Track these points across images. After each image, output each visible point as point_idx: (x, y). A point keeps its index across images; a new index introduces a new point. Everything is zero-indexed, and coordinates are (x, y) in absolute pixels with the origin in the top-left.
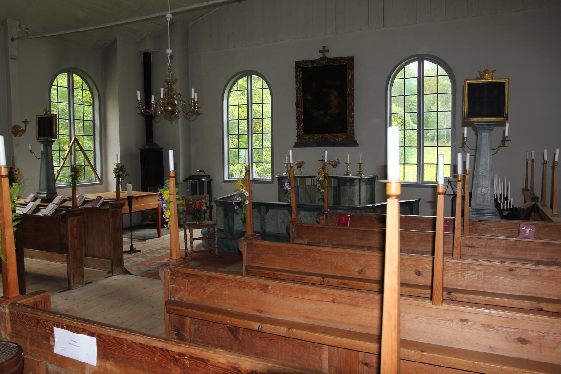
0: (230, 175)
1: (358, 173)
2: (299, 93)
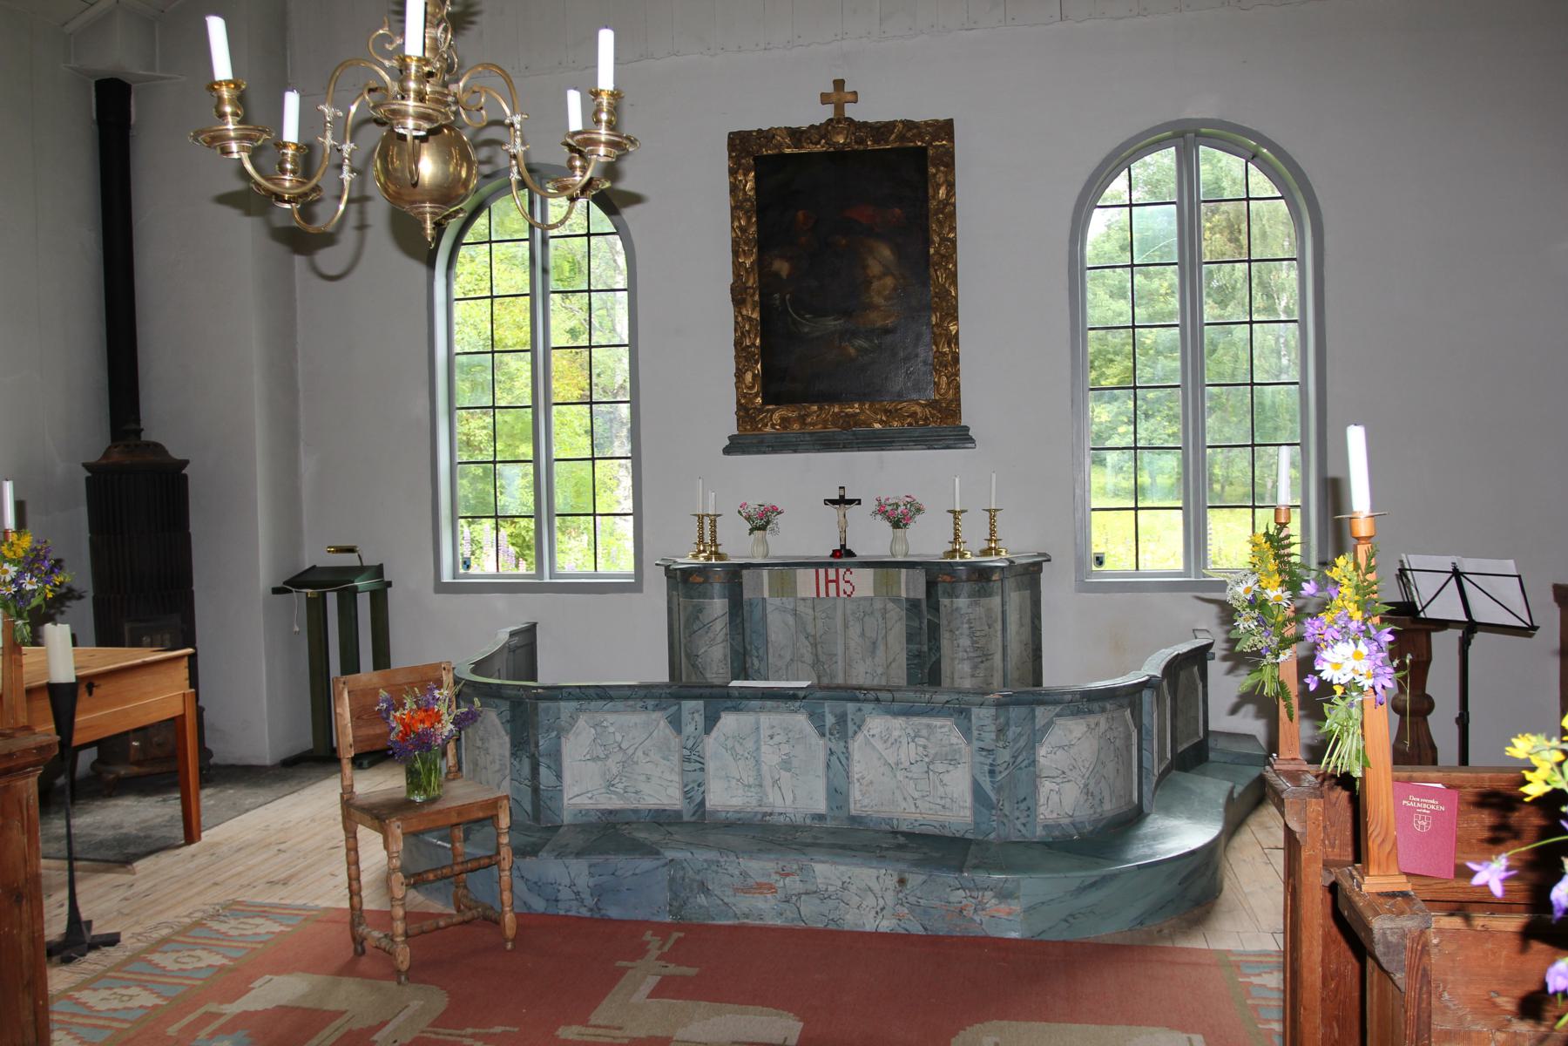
1: (986, 547)
2: (744, 251)
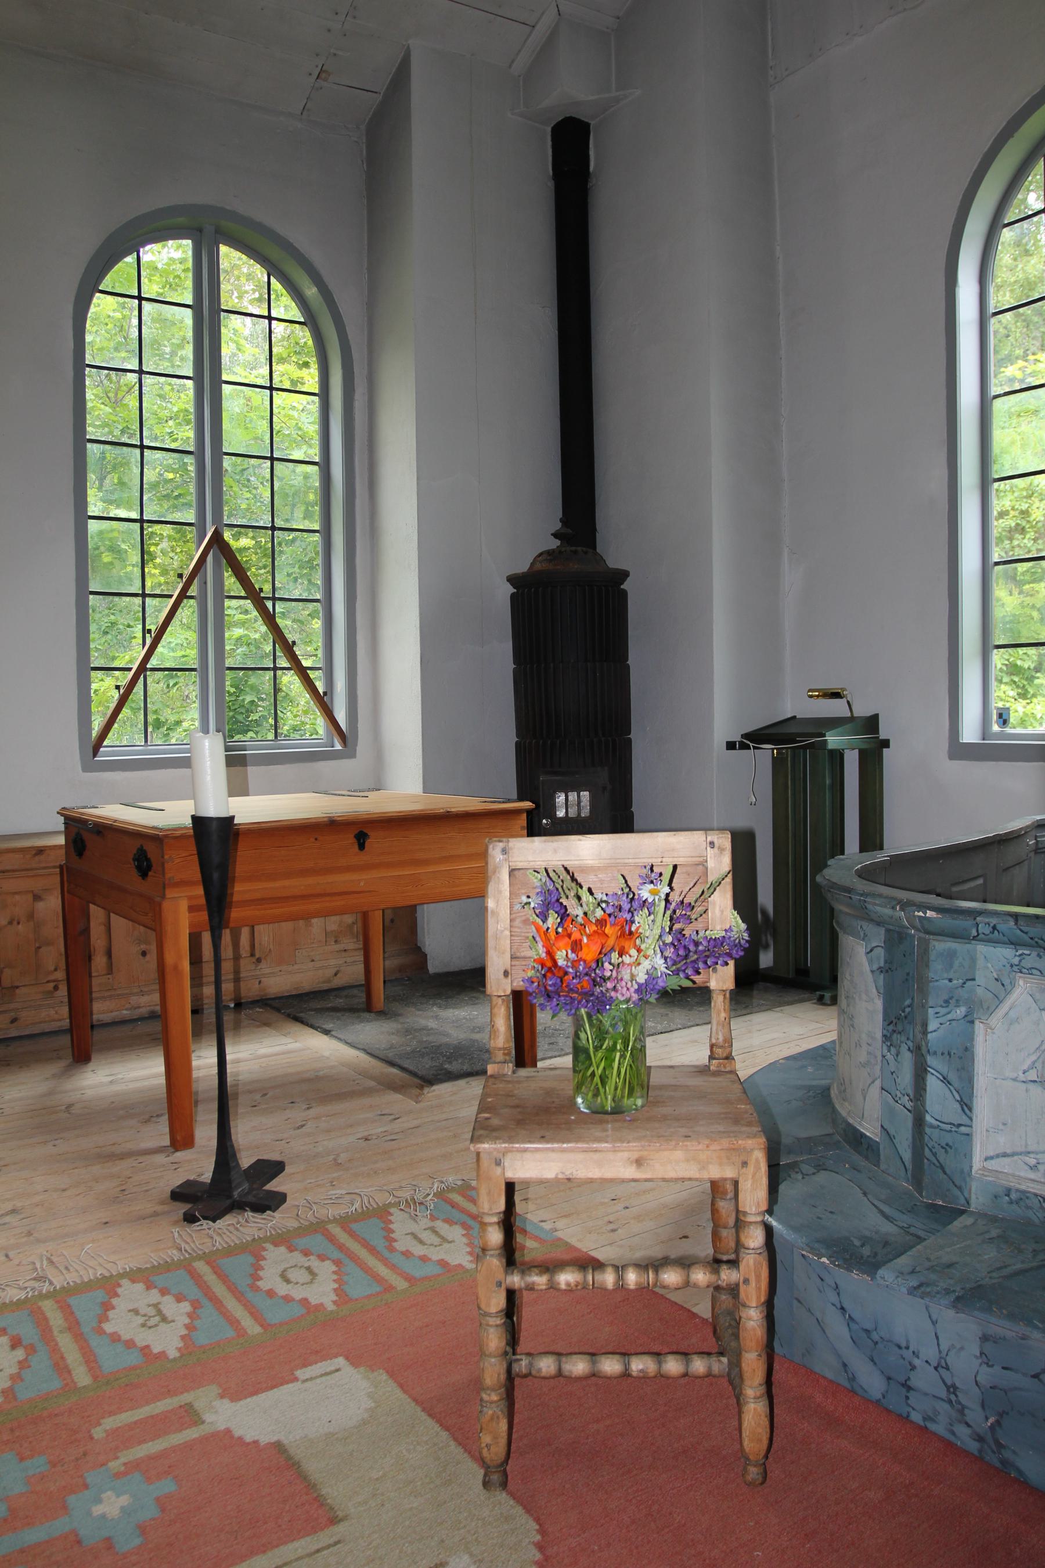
0: (995, 717)
